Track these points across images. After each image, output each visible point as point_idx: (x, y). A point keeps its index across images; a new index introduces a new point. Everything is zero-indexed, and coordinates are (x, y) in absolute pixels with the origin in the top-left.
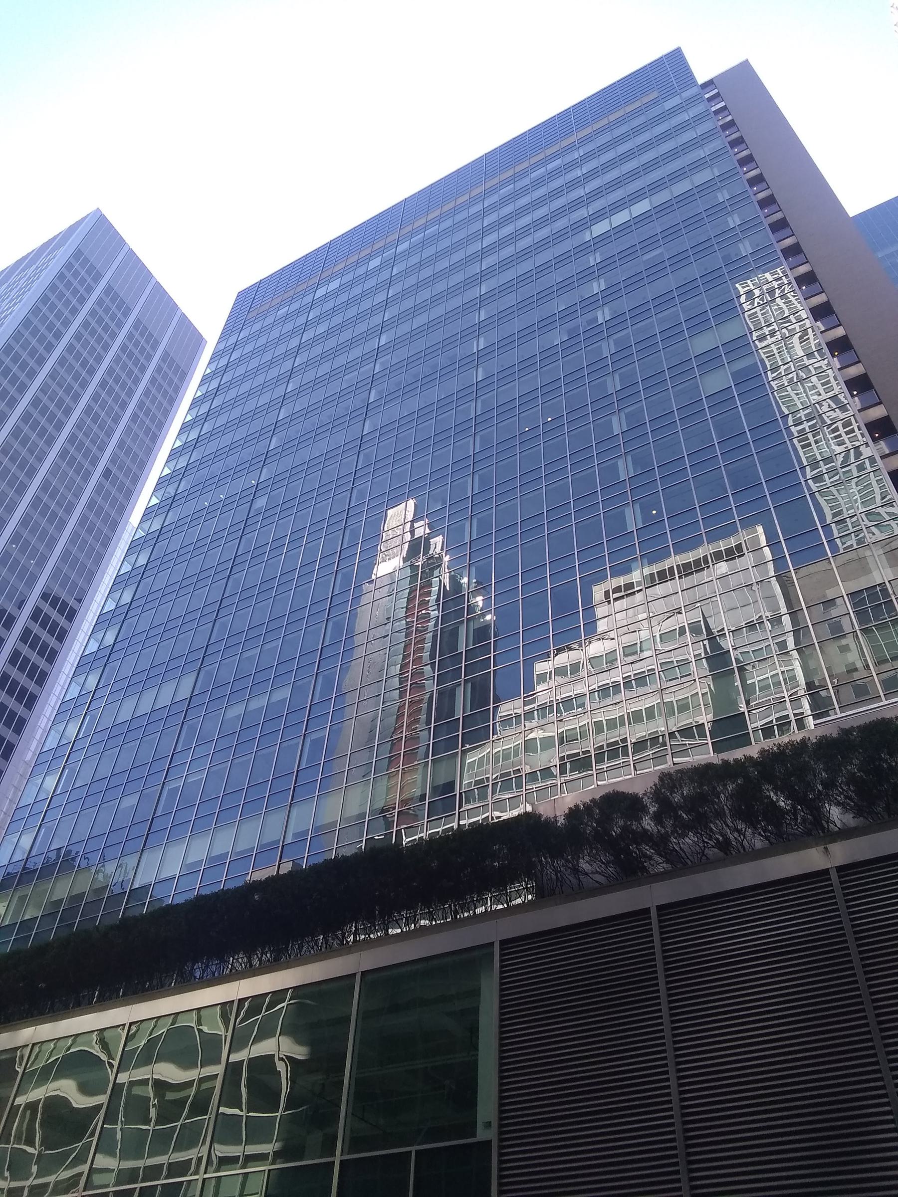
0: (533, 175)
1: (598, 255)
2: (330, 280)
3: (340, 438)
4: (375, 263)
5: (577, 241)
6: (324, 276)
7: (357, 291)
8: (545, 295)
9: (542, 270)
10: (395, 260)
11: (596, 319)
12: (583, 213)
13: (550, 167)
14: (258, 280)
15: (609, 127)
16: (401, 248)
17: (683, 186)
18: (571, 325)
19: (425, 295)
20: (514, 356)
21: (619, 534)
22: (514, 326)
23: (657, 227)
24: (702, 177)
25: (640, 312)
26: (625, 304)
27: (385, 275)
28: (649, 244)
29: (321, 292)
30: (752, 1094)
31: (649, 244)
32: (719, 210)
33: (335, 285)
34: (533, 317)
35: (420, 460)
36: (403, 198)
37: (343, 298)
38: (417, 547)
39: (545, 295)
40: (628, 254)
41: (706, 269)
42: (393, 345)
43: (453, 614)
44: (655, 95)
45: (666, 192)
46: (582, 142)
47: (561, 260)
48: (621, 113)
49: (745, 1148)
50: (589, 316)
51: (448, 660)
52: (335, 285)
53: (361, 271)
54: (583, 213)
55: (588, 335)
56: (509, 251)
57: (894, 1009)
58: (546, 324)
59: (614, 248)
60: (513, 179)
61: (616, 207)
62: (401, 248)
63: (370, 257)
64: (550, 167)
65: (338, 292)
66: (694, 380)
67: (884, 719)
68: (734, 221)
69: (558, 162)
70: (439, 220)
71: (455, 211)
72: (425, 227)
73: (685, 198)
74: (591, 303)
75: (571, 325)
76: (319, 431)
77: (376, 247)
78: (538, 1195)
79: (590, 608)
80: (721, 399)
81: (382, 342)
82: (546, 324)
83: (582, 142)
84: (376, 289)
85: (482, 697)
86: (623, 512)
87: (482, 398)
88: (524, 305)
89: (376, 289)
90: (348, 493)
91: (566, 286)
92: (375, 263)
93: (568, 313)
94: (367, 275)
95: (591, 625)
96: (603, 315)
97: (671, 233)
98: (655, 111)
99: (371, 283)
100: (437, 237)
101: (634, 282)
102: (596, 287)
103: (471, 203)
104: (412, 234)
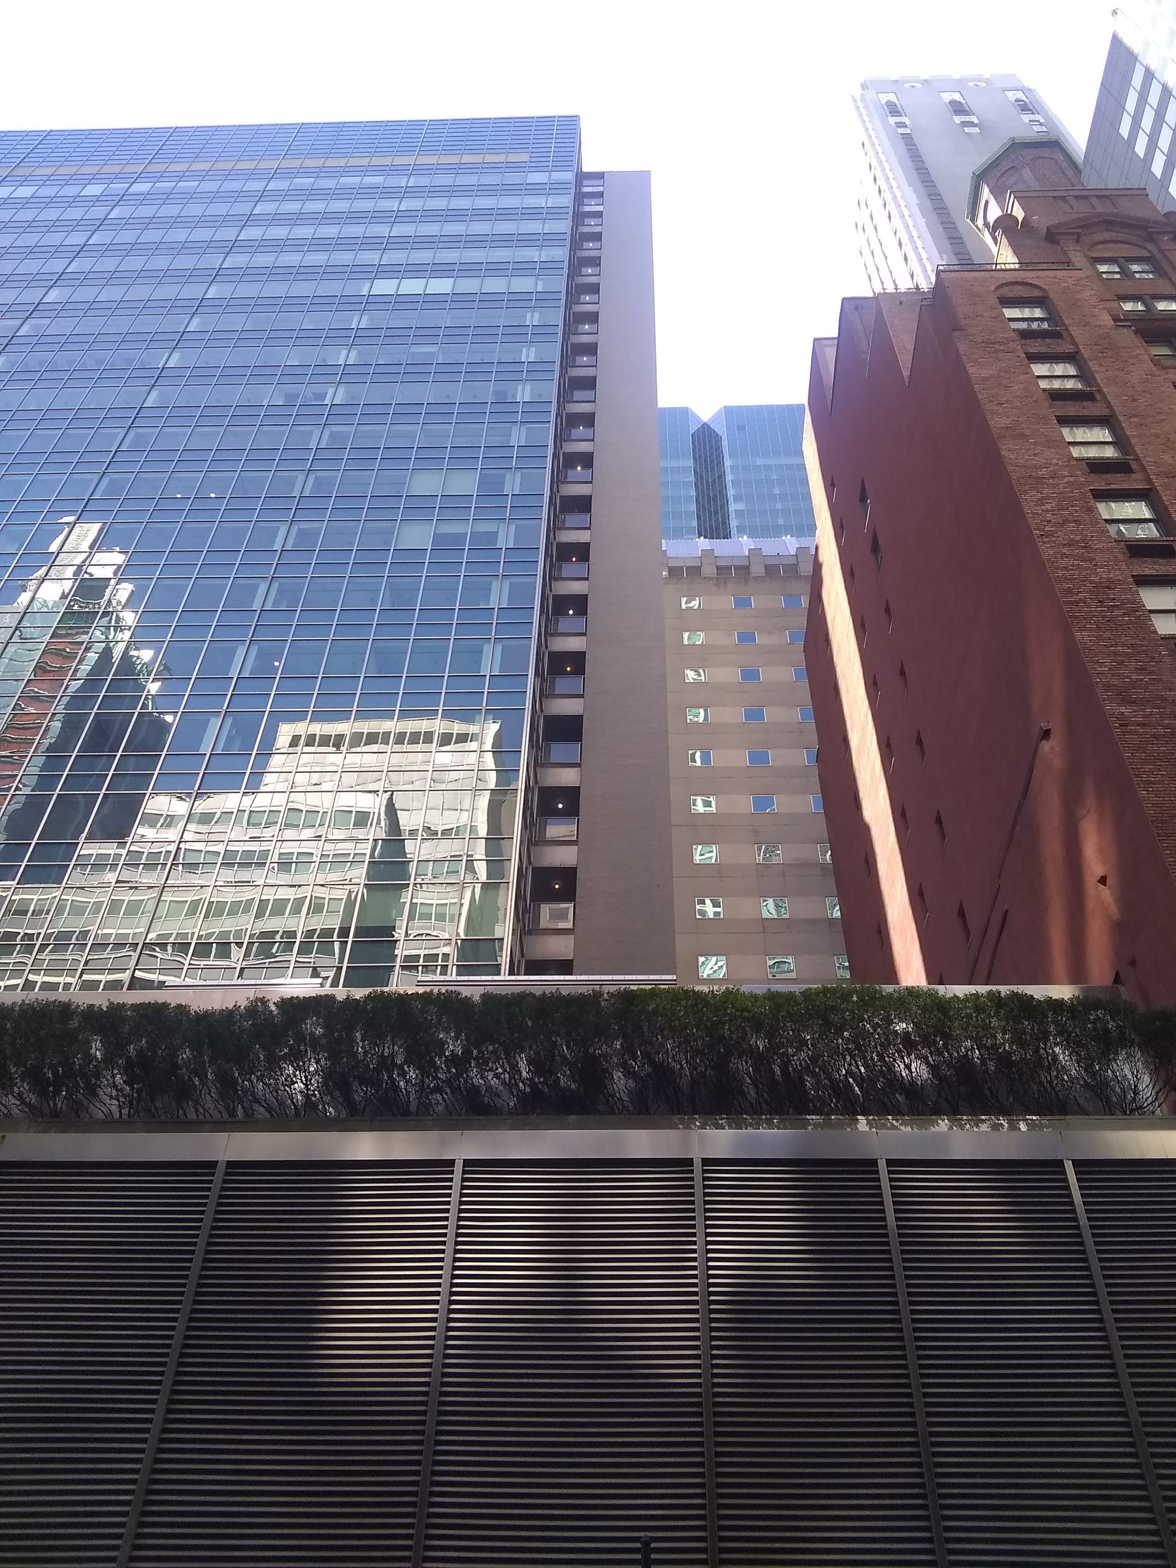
0: (343, 180)
1: (536, 315)
2: (24, 181)
3: (108, 397)
4: (94, 190)
5: (351, 288)
6: (151, 168)
7: (52, 214)
8: (276, 337)
9: (289, 303)
10: (121, 199)
11: (325, 395)
12: (372, 257)
13: (368, 180)
14: (49, 128)
15: (458, 169)
16: (137, 188)
17: (495, 285)
18: (290, 389)
19: (135, 263)
20: (204, 396)
21: (468, 676)
22: (225, 357)
23: (446, 319)
24: (523, 284)
25: (375, 412)
26: (365, 394)
27: (99, 212)
28: (426, 334)
29: (141, 187)
30: (582, 1450)
31: (426, 334)
32: (517, 333)
33: (25, 192)
34: (253, 356)
35: (82, 476)
36: (300, 121)
37: (27, 215)
38: (90, 587)
39: (276, 337)
40: (396, 335)
41: (540, 396)
42: (62, 309)
43: (127, 700)
44: (525, 157)
45: (477, 281)
46: (416, 170)
47: (317, 303)
48: (477, 159)
49: (892, 1529)
50: (320, 388)
51: (133, 759)
52: (25, 192)
53: (71, 191)
54: (372, 257)
55: (304, 411)
56: (318, 258)
57: (1171, 1389)
58: (262, 374)
59: (386, 319)
60: (319, 173)
61: (497, 269)
62: (137, 188)
63: (92, 179)
64: (368, 180)
65: (26, 203)
66: (389, 524)
67: (156, 1004)
68: (529, 354)
69: (379, 180)
70: (203, 177)
71: (228, 176)
72: (182, 176)
73: (489, 300)
74: (325, 372)
75: (290, 389)
76: (76, 375)
77: (106, 170)
78: (1068, 1565)
79: (266, 753)
80: (409, 559)
81: (50, 298)
82: (262, 374)
83: (416, 170)
84: (76, 225)
85: (67, 823)
86: (235, 650)
87: (139, 430)
88: (243, 338)
89: (76, 225)
90: (96, 478)
91: (304, 337)
92: (94, 190)
93: (294, 374)
94: (75, 200)
95: (258, 775)
96: (336, 395)
97: (455, 334)
98: (513, 178)
99: (75, 213)
100: (191, 197)
101: (387, 373)
102: (343, 356)
103: (252, 175)
104: (161, 177)
